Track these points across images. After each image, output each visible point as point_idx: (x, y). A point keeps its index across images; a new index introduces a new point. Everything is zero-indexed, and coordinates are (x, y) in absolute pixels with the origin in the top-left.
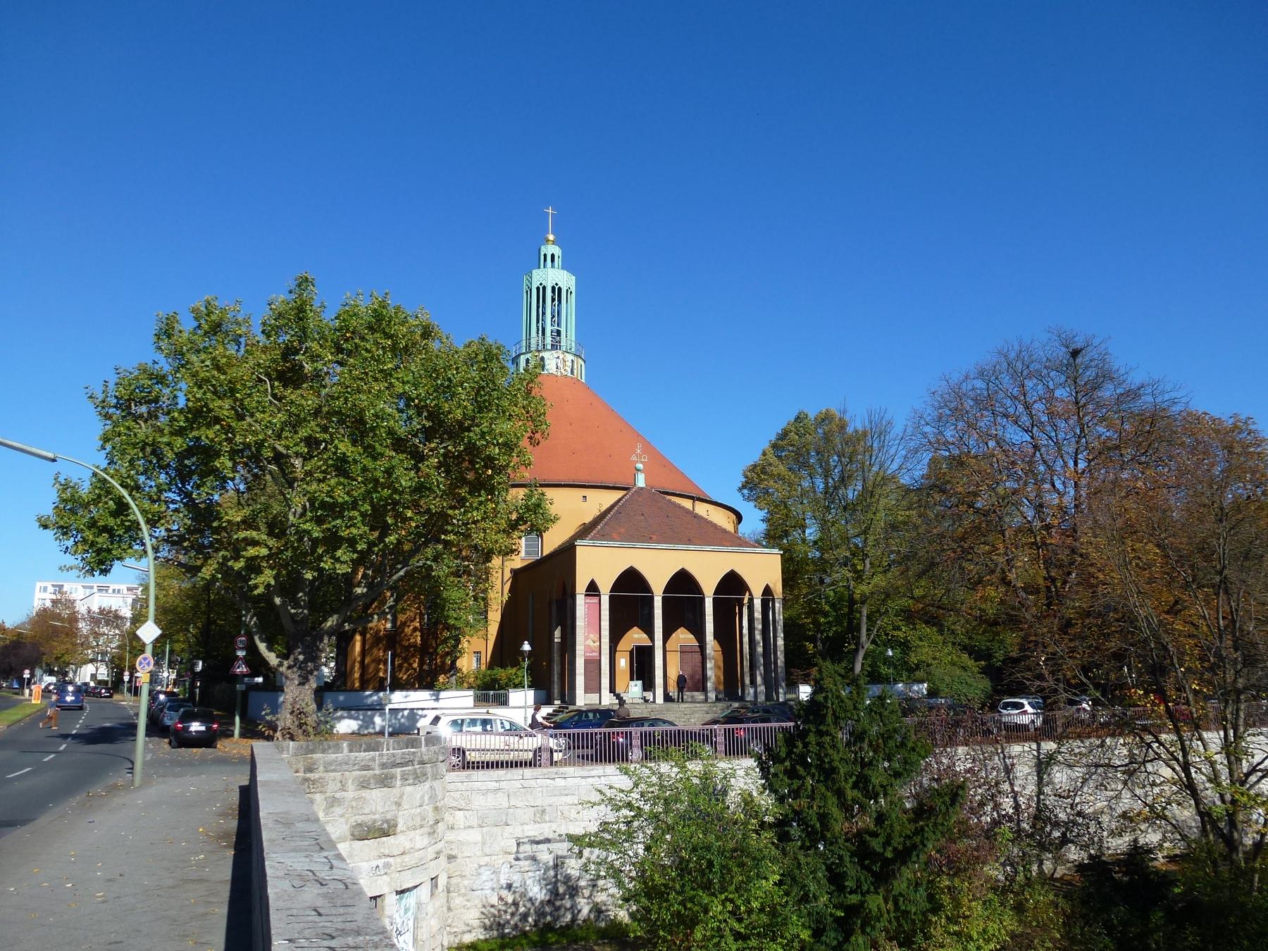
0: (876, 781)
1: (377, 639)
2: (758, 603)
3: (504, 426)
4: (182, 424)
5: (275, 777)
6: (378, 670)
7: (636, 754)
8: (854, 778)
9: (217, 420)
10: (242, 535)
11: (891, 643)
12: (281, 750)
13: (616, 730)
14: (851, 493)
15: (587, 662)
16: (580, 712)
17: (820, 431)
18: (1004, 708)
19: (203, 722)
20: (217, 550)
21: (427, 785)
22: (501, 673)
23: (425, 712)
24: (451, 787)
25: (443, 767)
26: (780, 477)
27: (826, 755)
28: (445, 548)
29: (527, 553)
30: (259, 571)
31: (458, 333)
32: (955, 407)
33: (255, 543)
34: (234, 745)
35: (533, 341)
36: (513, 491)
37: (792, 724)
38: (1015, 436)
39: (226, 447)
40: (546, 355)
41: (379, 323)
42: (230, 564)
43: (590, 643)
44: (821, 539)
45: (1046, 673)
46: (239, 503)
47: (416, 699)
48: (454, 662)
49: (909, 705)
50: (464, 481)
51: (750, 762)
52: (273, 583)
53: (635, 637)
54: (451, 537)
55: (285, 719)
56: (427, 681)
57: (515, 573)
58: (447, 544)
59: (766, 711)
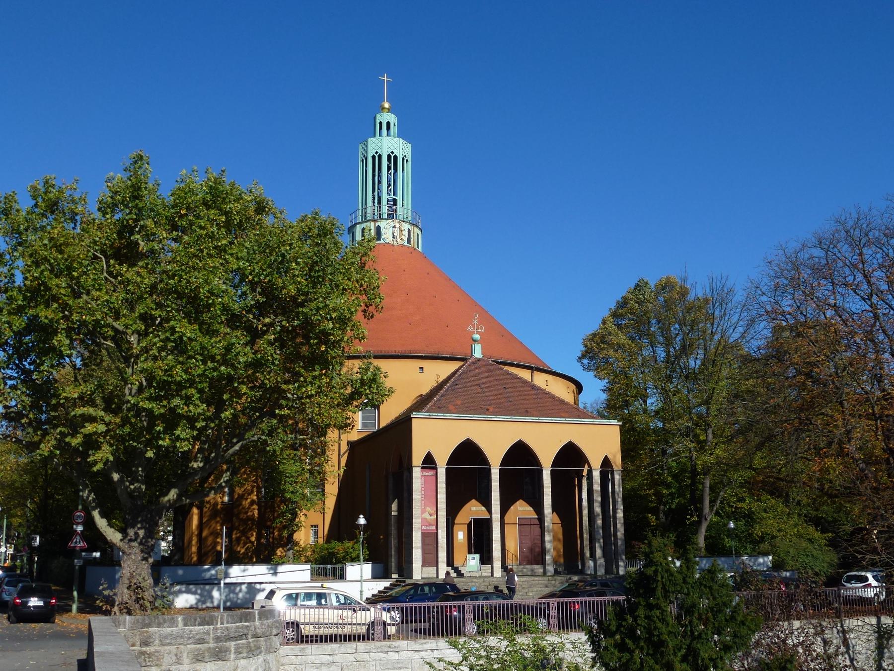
0: (704, 655)
1: (215, 513)
2: (596, 475)
3: (337, 301)
4: (20, 303)
5: (110, 648)
6: (216, 544)
7: (471, 628)
8: (683, 651)
9: (55, 298)
10: (79, 411)
11: (736, 515)
12: (117, 624)
13: (448, 603)
14: (694, 362)
15: (425, 535)
16: (416, 586)
17: (661, 298)
18: (848, 581)
19: (41, 597)
20: (55, 427)
21: (261, 659)
22: (338, 547)
23: (263, 586)
24: (285, 660)
25: (276, 641)
26: (620, 347)
27: (655, 628)
28: (279, 422)
29: (364, 425)
30: (98, 447)
31: (290, 210)
32: (793, 276)
33: (92, 419)
34: (72, 620)
35: (369, 211)
36: (349, 363)
37: (624, 597)
38: (855, 304)
39: (63, 325)
40: (382, 224)
41: (216, 197)
42: (67, 440)
43: (426, 516)
44: (663, 409)
45: (879, 547)
46: (76, 380)
47: (256, 573)
48: (291, 536)
49: (744, 580)
50: (298, 356)
51: (583, 637)
52: (111, 458)
53: (473, 510)
54: (286, 412)
55: (123, 594)
56: (264, 555)
57: (352, 445)
58: (282, 418)
59: (604, 584)
